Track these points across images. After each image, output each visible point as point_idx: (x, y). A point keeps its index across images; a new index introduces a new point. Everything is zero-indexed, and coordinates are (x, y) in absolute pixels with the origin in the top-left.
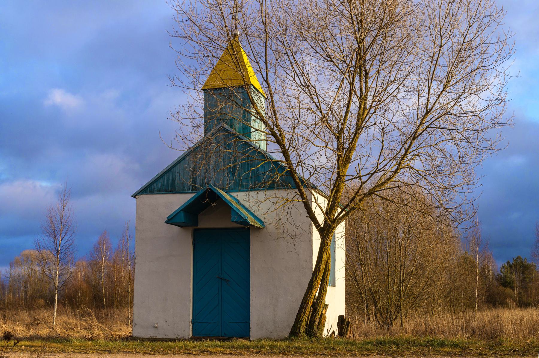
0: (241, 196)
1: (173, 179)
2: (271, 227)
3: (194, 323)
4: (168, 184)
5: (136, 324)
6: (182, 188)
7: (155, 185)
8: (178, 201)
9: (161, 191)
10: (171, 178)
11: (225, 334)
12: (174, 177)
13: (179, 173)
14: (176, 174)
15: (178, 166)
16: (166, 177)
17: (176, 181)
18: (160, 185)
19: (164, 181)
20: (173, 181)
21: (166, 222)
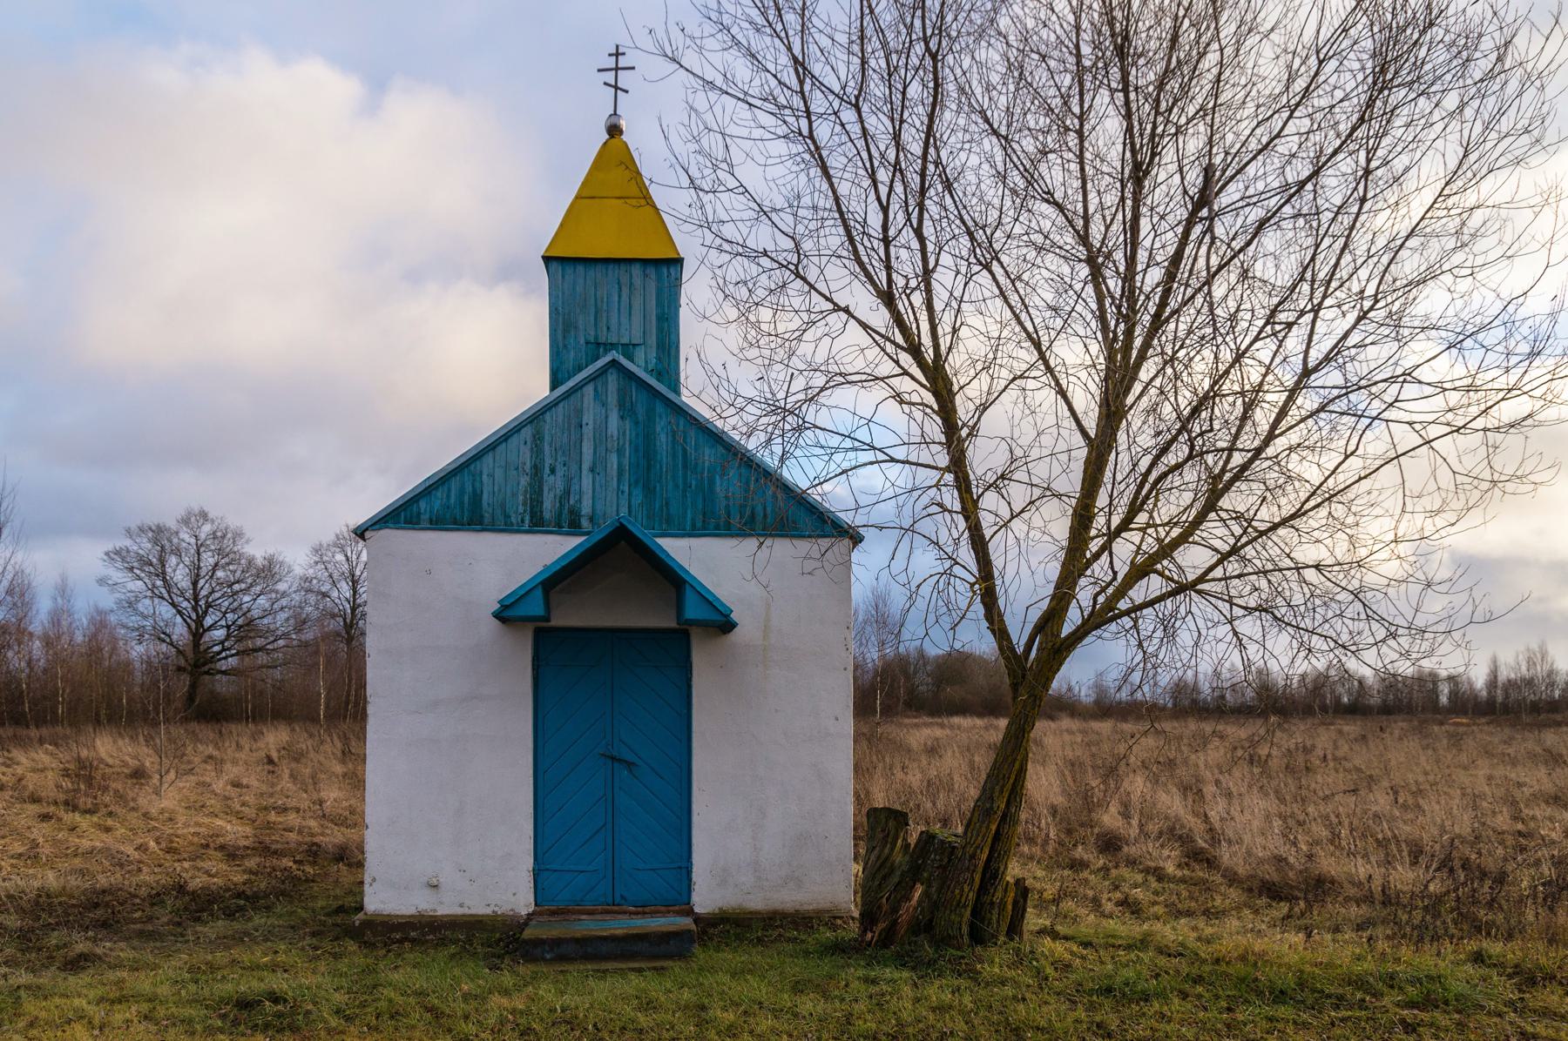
0: (660, 541)
1: (474, 490)
2: (747, 628)
3: (537, 874)
4: (462, 503)
5: (374, 880)
6: (501, 518)
7: (423, 504)
8: (522, 558)
9: (439, 523)
10: (469, 489)
11: (622, 897)
12: (478, 485)
13: (491, 476)
14: (485, 477)
15: (489, 459)
16: (454, 484)
17: (485, 496)
18: (437, 505)
19: (448, 497)
20: (476, 498)
21: (64, 579)
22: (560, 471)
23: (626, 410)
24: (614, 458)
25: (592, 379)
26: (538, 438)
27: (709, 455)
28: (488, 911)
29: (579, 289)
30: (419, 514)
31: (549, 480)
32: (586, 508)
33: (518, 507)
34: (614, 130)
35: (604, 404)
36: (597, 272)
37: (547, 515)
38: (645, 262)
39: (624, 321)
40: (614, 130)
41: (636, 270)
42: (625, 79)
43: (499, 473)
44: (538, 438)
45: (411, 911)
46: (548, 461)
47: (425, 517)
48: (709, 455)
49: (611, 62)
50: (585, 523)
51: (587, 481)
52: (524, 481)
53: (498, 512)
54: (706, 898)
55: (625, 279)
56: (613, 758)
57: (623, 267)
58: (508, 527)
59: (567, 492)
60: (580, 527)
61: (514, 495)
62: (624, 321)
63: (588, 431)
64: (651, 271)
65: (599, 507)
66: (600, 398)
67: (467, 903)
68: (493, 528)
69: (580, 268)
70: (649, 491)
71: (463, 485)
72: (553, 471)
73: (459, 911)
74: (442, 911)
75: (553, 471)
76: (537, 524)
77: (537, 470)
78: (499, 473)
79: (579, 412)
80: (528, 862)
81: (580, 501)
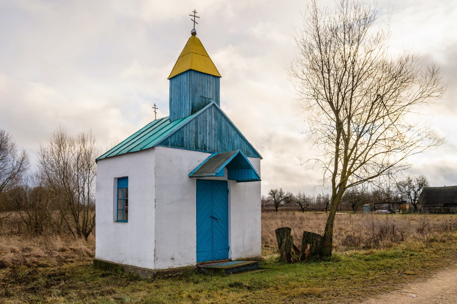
4: (179, 140)
9: (174, 146)
10: (181, 135)
13: (186, 133)
16: (177, 134)
17: (185, 139)
20: (183, 139)
22: (202, 133)
23: (216, 119)
24: (213, 131)
25: (209, 108)
26: (196, 123)
27: (233, 133)
28: (186, 265)
29: (198, 80)
30: (168, 143)
31: (199, 136)
32: (208, 146)
33: (192, 144)
34: (194, 34)
35: (211, 116)
36: (203, 76)
37: (199, 146)
38: (213, 76)
39: (209, 92)
40: (194, 34)
41: (211, 77)
42: (197, 19)
43: (188, 132)
44: (196, 123)
45: (167, 268)
46: (199, 130)
47: (170, 144)
48: (233, 133)
49: (193, 14)
50: (208, 149)
51: (208, 137)
52: (194, 135)
53: (188, 144)
54: (234, 255)
55: (209, 80)
56: (213, 218)
57: (209, 76)
58: (190, 149)
59: (203, 140)
60: (206, 150)
61: (192, 139)
62: (209, 92)
63: (208, 122)
64: (214, 79)
65: (210, 145)
66: (210, 113)
67: (181, 263)
68: (186, 149)
69: (199, 74)
70: (221, 141)
71: (179, 135)
72: (200, 133)
73: (179, 266)
74: (175, 267)
75: (200, 133)
76: (197, 149)
77: (196, 132)
78: (188, 132)
79: (206, 117)
80: (195, 250)
81: (206, 143)
